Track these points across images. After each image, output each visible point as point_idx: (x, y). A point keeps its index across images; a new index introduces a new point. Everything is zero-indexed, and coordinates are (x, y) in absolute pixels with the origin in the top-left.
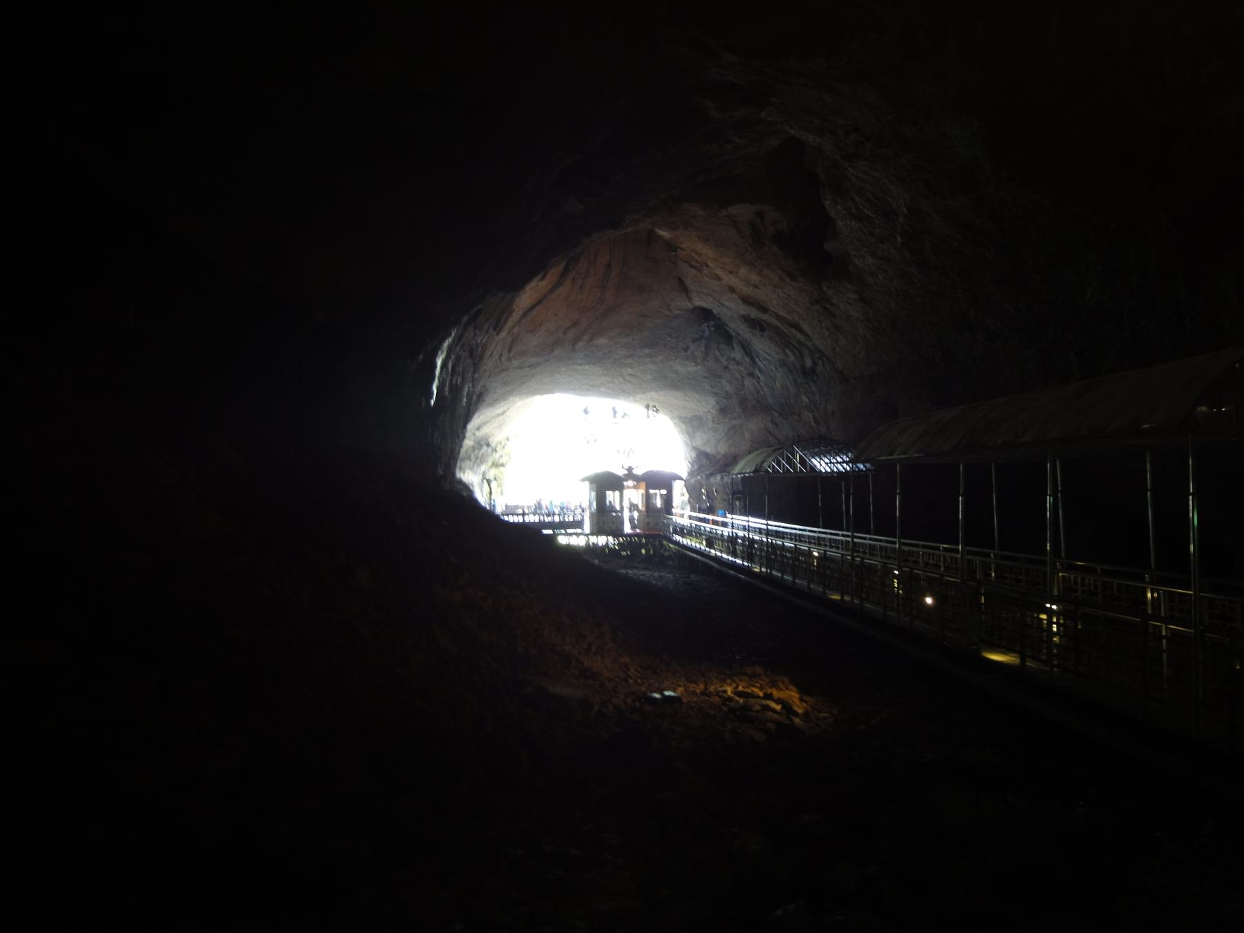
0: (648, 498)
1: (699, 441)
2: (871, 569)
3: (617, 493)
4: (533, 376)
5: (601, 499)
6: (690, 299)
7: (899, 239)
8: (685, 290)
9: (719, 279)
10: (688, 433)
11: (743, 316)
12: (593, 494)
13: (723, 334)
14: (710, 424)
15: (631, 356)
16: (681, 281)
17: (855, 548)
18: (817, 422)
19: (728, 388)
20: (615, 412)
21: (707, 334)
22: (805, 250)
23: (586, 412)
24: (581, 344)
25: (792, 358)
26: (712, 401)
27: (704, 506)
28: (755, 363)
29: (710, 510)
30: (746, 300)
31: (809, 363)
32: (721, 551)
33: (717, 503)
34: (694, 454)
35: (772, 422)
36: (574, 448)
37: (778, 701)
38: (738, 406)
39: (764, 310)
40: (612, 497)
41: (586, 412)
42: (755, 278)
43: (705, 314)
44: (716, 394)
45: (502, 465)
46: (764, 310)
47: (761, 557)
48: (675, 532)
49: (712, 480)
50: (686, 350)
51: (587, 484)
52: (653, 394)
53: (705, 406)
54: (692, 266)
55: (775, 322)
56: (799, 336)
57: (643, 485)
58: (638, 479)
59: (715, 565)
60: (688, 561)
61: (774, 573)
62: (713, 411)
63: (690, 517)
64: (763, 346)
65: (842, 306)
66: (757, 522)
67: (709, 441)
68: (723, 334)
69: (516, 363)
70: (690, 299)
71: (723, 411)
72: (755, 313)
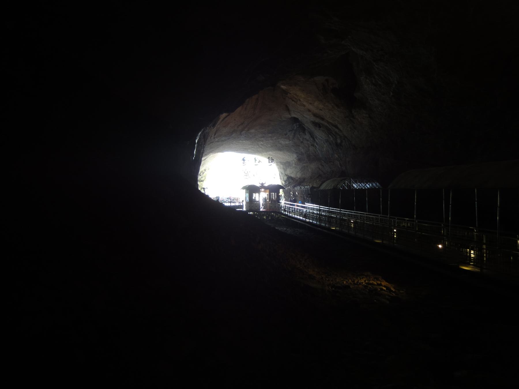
0: (270, 195)
1: (288, 172)
2: (345, 220)
3: (257, 194)
4: (222, 145)
5: (251, 196)
6: (290, 114)
7: (391, 94)
8: (288, 110)
9: (304, 106)
10: (284, 169)
11: (312, 121)
12: (248, 194)
13: (302, 128)
14: (294, 165)
15: (263, 137)
16: (287, 106)
17: (320, 210)
18: (340, 165)
19: (302, 150)
20: (256, 160)
21: (295, 128)
22: (346, 96)
23: (244, 160)
24: (244, 132)
25: (332, 139)
26: (295, 156)
27: (292, 199)
28: (315, 141)
29: (295, 201)
30: (315, 115)
31: (339, 141)
32: (300, 216)
33: (298, 198)
34: (286, 178)
35: (321, 165)
36: (236, 174)
37: (385, 286)
38: (305, 158)
39: (323, 119)
40: (256, 196)
41: (244, 160)
42: (321, 106)
43: (295, 120)
44: (297, 153)
45: (202, 181)
46: (323, 119)
47: (316, 218)
48: (285, 211)
49: (296, 189)
50: (286, 135)
51: (244, 190)
52: (270, 153)
53: (292, 157)
54: (293, 101)
55: (326, 124)
56: (337, 130)
57: (268, 191)
58: (266, 188)
59: (309, 225)
60: (289, 221)
61: (343, 230)
62: (295, 160)
63: (285, 203)
64: (320, 134)
65: (359, 120)
66: (315, 206)
67: (293, 172)
68: (302, 128)
69: (217, 140)
70: (290, 114)
71: (300, 160)
72: (317, 120)
